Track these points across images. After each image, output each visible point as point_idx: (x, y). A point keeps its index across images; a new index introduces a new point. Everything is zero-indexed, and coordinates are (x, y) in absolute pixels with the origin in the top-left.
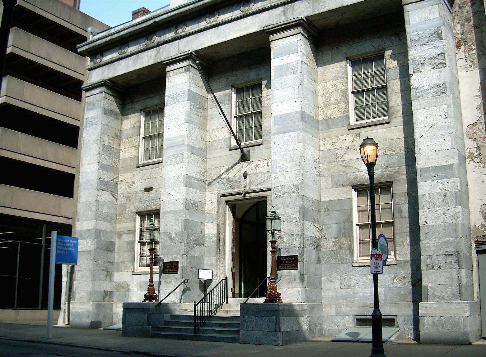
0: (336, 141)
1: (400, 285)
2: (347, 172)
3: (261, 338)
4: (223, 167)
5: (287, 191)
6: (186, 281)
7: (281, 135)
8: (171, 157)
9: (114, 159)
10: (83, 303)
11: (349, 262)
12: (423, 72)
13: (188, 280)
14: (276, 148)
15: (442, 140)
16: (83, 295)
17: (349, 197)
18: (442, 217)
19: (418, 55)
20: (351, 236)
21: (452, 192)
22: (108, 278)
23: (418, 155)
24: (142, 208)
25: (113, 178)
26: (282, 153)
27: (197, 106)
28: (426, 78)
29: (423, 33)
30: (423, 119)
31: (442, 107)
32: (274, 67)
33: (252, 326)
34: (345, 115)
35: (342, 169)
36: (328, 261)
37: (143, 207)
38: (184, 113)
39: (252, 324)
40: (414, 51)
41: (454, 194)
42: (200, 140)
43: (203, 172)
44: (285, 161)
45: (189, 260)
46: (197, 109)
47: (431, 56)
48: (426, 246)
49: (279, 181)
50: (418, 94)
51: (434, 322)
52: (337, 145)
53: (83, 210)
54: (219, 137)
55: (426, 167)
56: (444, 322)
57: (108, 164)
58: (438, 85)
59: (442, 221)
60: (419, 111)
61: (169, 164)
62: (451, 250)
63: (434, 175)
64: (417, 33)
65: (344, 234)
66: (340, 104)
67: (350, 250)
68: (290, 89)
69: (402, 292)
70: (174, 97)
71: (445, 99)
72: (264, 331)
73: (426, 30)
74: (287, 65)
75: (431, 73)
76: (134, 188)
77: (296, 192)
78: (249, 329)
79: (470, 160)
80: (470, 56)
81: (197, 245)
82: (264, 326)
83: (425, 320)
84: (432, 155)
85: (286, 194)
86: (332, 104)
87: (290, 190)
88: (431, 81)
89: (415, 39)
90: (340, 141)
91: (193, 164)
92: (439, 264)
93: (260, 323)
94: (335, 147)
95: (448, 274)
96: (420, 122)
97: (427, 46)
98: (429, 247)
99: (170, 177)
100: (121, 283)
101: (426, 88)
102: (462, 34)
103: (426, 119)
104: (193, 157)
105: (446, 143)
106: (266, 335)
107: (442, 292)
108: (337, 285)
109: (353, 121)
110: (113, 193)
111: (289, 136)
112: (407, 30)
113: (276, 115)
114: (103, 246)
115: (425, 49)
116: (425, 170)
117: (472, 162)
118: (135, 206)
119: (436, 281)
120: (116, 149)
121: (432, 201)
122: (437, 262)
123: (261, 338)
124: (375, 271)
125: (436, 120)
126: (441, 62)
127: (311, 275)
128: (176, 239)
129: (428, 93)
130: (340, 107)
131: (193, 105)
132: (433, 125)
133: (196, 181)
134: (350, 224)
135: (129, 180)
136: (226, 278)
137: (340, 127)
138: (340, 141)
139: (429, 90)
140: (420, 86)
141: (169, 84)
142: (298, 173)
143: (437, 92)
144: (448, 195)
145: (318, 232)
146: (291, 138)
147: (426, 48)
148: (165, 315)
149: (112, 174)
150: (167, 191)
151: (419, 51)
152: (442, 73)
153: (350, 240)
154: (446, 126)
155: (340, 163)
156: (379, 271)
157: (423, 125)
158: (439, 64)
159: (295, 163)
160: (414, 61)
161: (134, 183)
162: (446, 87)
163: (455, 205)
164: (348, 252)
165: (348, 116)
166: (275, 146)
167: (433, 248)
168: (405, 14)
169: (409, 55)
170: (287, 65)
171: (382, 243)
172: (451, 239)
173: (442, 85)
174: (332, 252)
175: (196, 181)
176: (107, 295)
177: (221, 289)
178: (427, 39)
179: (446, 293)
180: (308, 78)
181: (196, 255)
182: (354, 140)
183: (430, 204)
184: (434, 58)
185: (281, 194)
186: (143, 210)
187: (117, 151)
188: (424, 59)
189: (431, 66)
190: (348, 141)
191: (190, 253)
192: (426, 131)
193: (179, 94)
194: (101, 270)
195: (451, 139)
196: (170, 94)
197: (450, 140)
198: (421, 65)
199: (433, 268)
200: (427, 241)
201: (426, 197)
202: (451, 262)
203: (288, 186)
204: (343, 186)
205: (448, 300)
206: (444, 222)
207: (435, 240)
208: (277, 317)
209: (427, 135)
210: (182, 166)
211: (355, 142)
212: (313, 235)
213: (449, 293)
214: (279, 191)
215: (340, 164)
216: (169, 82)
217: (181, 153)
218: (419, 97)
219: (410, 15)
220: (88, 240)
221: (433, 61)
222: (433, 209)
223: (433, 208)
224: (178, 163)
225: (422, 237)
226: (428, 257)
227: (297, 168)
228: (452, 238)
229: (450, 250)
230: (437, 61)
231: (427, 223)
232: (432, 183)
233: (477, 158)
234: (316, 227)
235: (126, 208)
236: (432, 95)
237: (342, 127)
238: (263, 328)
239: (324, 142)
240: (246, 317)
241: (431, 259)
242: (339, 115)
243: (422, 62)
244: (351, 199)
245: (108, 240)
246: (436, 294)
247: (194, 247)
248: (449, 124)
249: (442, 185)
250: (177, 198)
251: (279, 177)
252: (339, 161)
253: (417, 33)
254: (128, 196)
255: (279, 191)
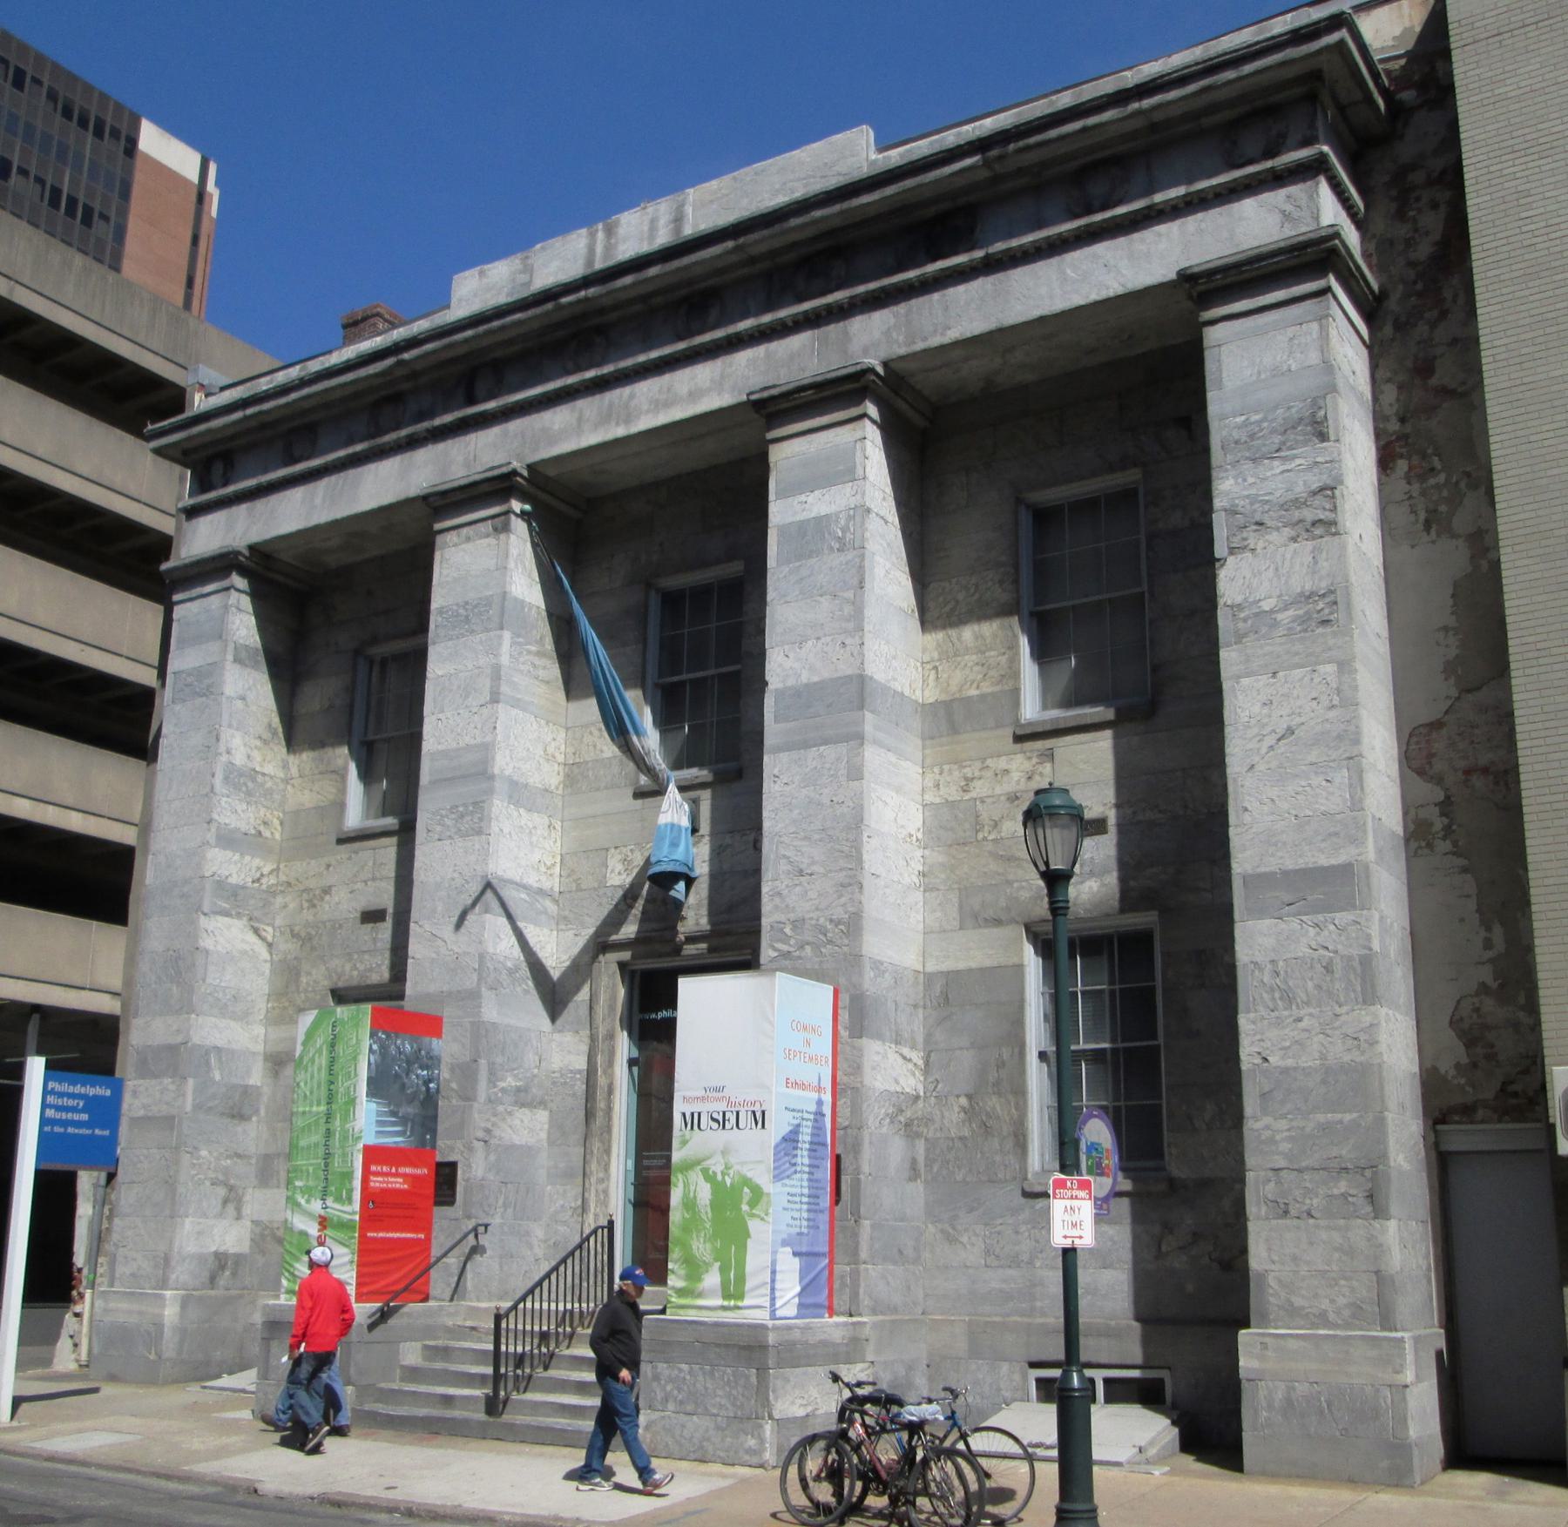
0: (977, 774)
1: (1179, 1262)
2: (1011, 877)
3: (708, 1440)
4: (613, 850)
5: (811, 939)
6: (481, 1229)
7: (795, 755)
8: (444, 812)
9: (263, 811)
10: (141, 1294)
11: (1015, 1178)
12: (1259, 551)
13: (486, 1226)
14: (778, 795)
15: (1318, 780)
16: (139, 1268)
17: (1015, 960)
18: (1315, 1039)
19: (1246, 493)
20: (1020, 1091)
21: (1350, 958)
22: (231, 1208)
23: (1239, 830)
24: (352, 977)
25: (258, 875)
26: (796, 812)
27: (533, 648)
28: (1270, 573)
29: (1264, 419)
30: (1257, 709)
31: (1322, 668)
32: (783, 530)
33: (680, 1397)
34: (1006, 688)
35: (993, 866)
36: (944, 1172)
37: (355, 973)
38: (489, 671)
39: (679, 1390)
40: (1231, 481)
41: (1356, 964)
42: (542, 761)
43: (549, 863)
44: (806, 838)
45: (492, 1158)
46: (531, 657)
47: (1290, 496)
48: (1263, 1137)
49: (787, 906)
50: (1241, 625)
51: (1289, 1402)
52: (979, 789)
53: (153, 978)
54: (602, 751)
55: (1262, 869)
56: (1324, 1405)
57: (244, 827)
58: (1309, 597)
59: (1317, 1055)
60: (1245, 681)
61: (437, 837)
62: (1346, 1152)
63: (1288, 898)
64: (1243, 418)
65: (997, 1084)
66: (992, 653)
67: (1016, 1136)
68: (825, 602)
69: (1190, 1288)
70: (458, 615)
71: (1331, 642)
72: (718, 1415)
73: (1276, 407)
74: (822, 523)
75: (1288, 556)
76: (326, 909)
77: (839, 942)
78: (671, 1406)
79: (1416, 844)
80: (1423, 493)
81: (523, 1105)
82: (718, 1399)
83: (1261, 1392)
84: (1283, 832)
85: (808, 949)
86: (967, 650)
87: (821, 937)
88: (1286, 582)
89: (1237, 437)
90: (989, 774)
91: (515, 837)
92: (1308, 1201)
93: (706, 1389)
94: (973, 794)
95: (1337, 1237)
96: (1246, 719)
97: (1276, 463)
98: (1272, 1141)
99: (438, 879)
100: (276, 1225)
101: (1266, 606)
102: (1403, 420)
103: (1265, 711)
104: (516, 814)
105: (1331, 790)
106: (723, 1430)
107: (1316, 1296)
108: (972, 1253)
109: (1031, 709)
110: (256, 925)
111: (821, 756)
112: (1213, 409)
113: (780, 686)
114: (216, 1102)
115: (1269, 474)
116: (1260, 881)
117: (1426, 851)
118: (327, 969)
119: (1295, 1259)
120: (271, 777)
121: (1282, 986)
122: (1297, 1193)
123: (708, 1440)
124: (1065, 1237)
125: (1300, 715)
126: (1322, 517)
127: (887, 1220)
128: (454, 1085)
129: (1275, 624)
130: (991, 660)
131: (519, 644)
132: (1290, 731)
133: (523, 896)
134: (1016, 1050)
135: (312, 883)
136: (611, 1223)
137: (992, 729)
138: (989, 774)
139: (1277, 612)
140: (1251, 600)
141: (445, 572)
142: (847, 881)
143: (1304, 620)
144: (1338, 966)
145: (914, 1075)
146: (827, 766)
147: (1272, 469)
148: (402, 1345)
149: (257, 862)
150: (427, 927)
151: (1251, 480)
152: (1324, 554)
153: (1017, 1103)
154: (1335, 734)
155: (990, 847)
156: (1081, 1237)
157: (1256, 730)
158: (1314, 524)
159: (837, 847)
160: (1232, 512)
161: (327, 891)
162: (1335, 603)
163: (1360, 1000)
164: (1009, 1144)
165: (1016, 693)
166: (777, 787)
167: (1285, 1147)
168: (1207, 354)
169: (1215, 493)
170: (819, 520)
171: (1094, 1139)
172: (1348, 1117)
173: (1324, 595)
174: (958, 1144)
175: (523, 896)
176: (222, 1267)
177: (599, 1257)
178: (1277, 439)
179: (1332, 1301)
180: (888, 565)
181: (517, 1140)
182: (1033, 772)
183: (1277, 995)
184: (1297, 503)
185: (791, 949)
186: (355, 983)
187: (276, 784)
188: (1266, 507)
189: (1288, 532)
190: (1015, 776)
191: (497, 1132)
192: (1264, 750)
193: (476, 606)
194: (208, 1183)
195: (1350, 778)
196: (445, 604)
197: (1346, 781)
198: (1255, 527)
199: (1286, 1212)
200: (1267, 1120)
201: (1261, 970)
202: (1344, 1196)
203: (813, 922)
204: (998, 922)
205: (1335, 1326)
206: (1323, 1057)
207: (1291, 1120)
208: (762, 1370)
209: (1268, 762)
210: (477, 846)
211: (1037, 778)
212: (893, 1088)
213: (1341, 1301)
214: (785, 939)
215: (990, 852)
216: (445, 565)
217: (475, 804)
218: (1245, 635)
219: (1223, 357)
220: (167, 1081)
221: (1297, 514)
222: (1286, 1013)
223: (1286, 1009)
224: (464, 835)
225: (1250, 1105)
226: (1271, 1174)
227: (842, 863)
228: (1350, 1111)
229: (1344, 1152)
230: (1309, 515)
231: (1265, 1060)
232: (1283, 925)
233: (1444, 838)
234: (904, 1058)
235: (298, 974)
236: (1289, 629)
237: (997, 727)
238: (714, 1406)
239: (938, 777)
240: (662, 1366)
241: (1279, 1182)
242: (987, 688)
243: (1258, 517)
244: (1019, 969)
245: (235, 1081)
246: (1298, 1301)
247: (510, 1113)
248: (1343, 727)
249: (1318, 934)
250: (460, 951)
251: (785, 892)
252: (985, 839)
253: (1243, 418)
254: (309, 934)
255: (785, 939)
